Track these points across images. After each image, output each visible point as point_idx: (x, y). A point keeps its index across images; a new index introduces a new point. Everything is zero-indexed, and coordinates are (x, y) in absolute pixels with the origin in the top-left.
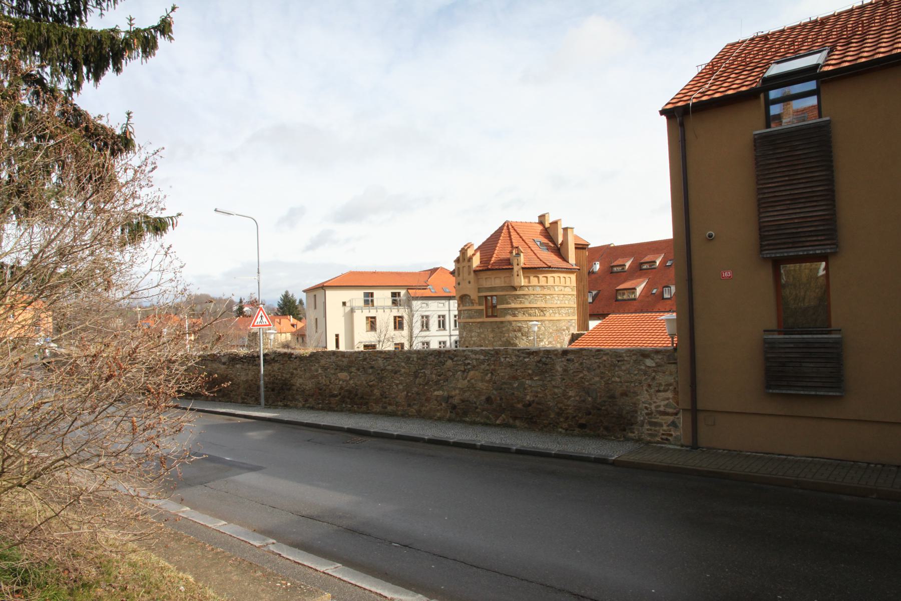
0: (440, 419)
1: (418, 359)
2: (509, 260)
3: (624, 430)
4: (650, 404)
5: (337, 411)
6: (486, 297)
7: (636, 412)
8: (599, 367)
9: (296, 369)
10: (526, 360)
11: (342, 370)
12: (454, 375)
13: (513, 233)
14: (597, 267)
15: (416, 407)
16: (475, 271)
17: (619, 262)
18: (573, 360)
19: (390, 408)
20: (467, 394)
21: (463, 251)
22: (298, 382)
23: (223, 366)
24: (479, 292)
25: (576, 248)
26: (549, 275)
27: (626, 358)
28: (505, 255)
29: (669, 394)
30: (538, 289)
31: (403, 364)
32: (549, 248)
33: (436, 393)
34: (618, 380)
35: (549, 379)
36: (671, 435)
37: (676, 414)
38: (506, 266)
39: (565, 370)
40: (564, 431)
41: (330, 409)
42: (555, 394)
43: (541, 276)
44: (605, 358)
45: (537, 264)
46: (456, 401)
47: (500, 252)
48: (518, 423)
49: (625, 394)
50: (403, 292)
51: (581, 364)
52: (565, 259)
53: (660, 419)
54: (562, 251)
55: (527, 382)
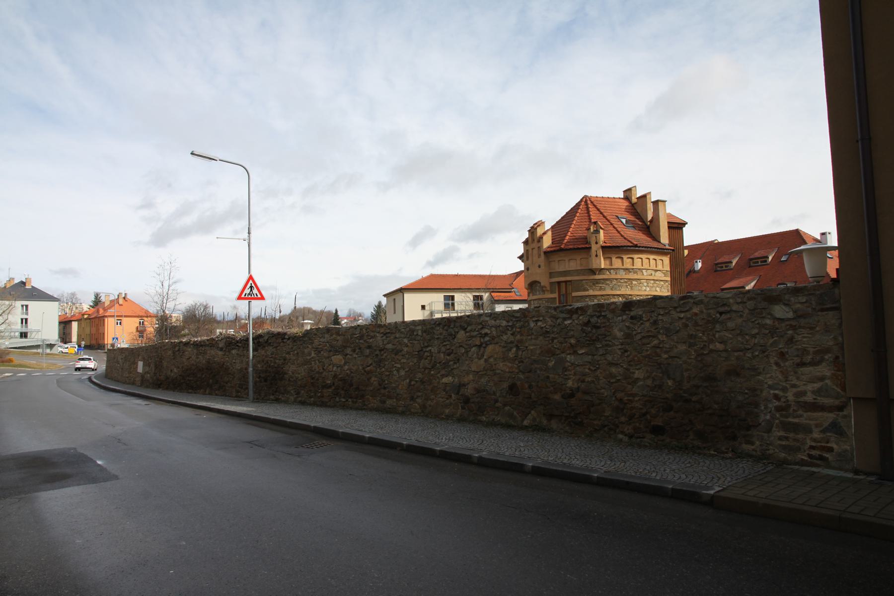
0: (448, 418)
1: (424, 331)
2: (586, 238)
3: (734, 438)
4: (785, 390)
5: (330, 407)
6: (559, 283)
7: (757, 405)
8: (686, 326)
9: (288, 353)
10: (567, 322)
11: (336, 352)
12: (467, 352)
13: (592, 210)
14: (699, 265)
15: (419, 400)
16: (545, 253)
17: (725, 259)
18: (641, 318)
19: (389, 402)
20: (484, 380)
21: (533, 230)
22: (291, 368)
23: (220, 353)
24: (550, 277)
25: (669, 227)
26: (635, 256)
27: (735, 308)
28: (581, 233)
29: (824, 370)
30: (622, 273)
31: (406, 341)
32: (635, 226)
33: (445, 380)
34: (720, 347)
35: (601, 352)
36: (830, 450)
37: (840, 408)
38: (582, 247)
39: (628, 336)
40: (626, 439)
41: (322, 404)
42: (611, 375)
43: (625, 257)
44: (696, 310)
45: (620, 242)
46: (469, 391)
47: (575, 230)
48: (554, 424)
49: (734, 372)
50: (486, 296)
51: (655, 323)
52: (656, 238)
53: (806, 418)
54: (651, 229)
55: (569, 358)
